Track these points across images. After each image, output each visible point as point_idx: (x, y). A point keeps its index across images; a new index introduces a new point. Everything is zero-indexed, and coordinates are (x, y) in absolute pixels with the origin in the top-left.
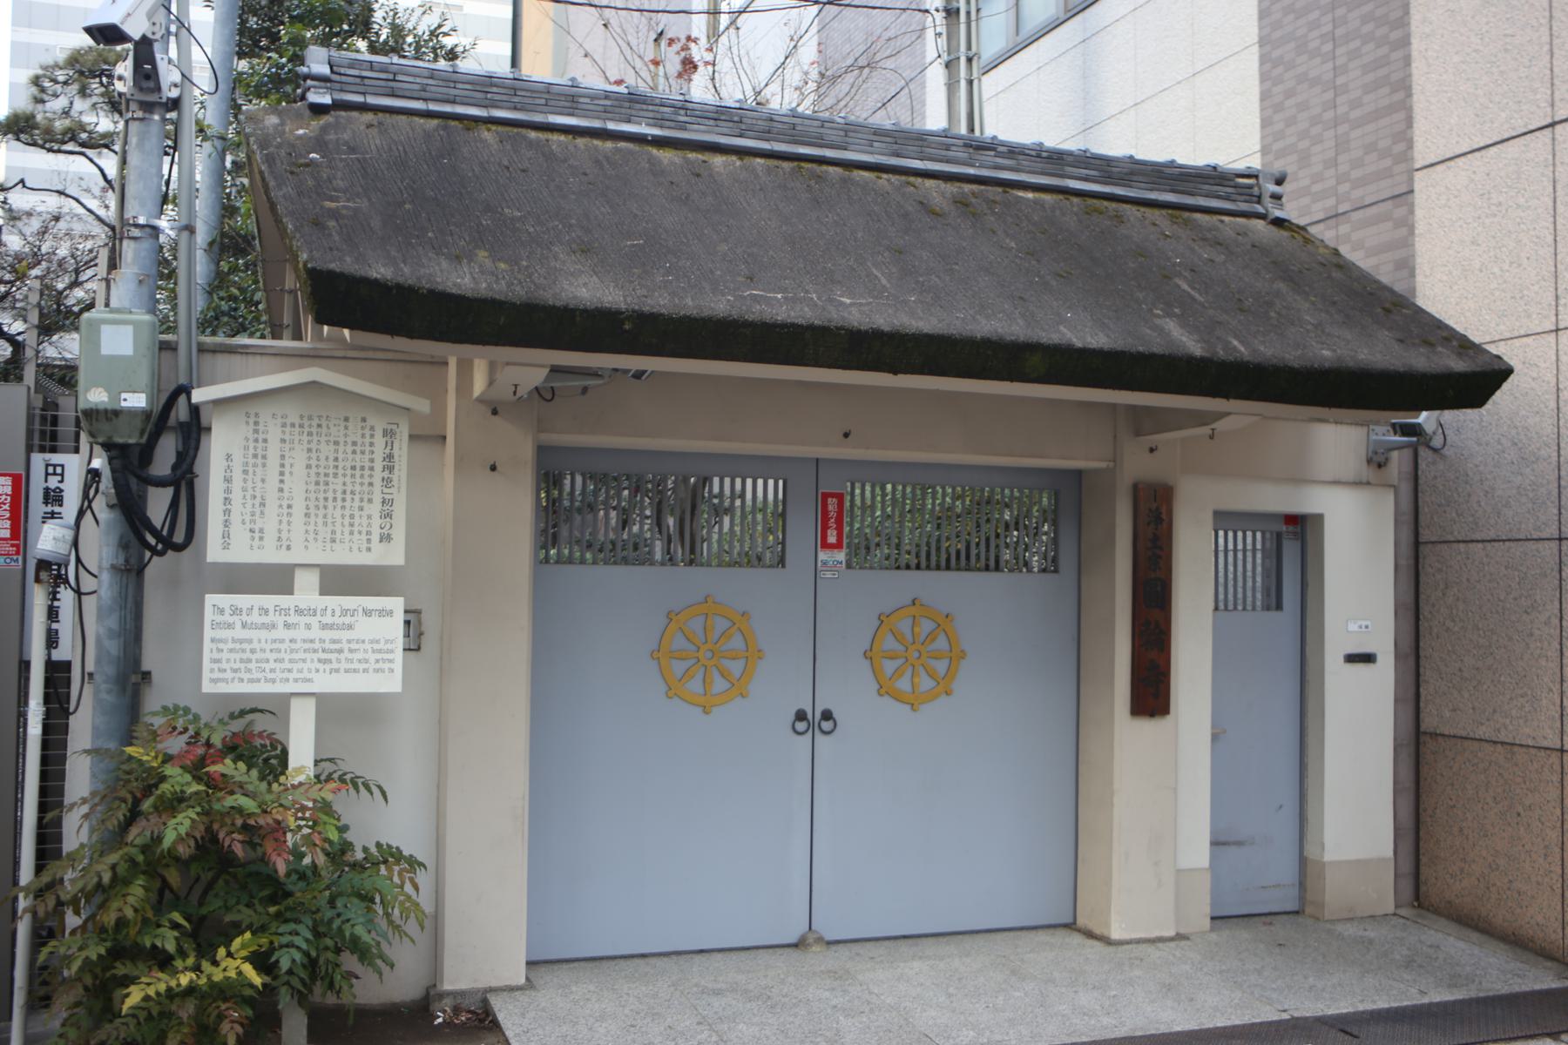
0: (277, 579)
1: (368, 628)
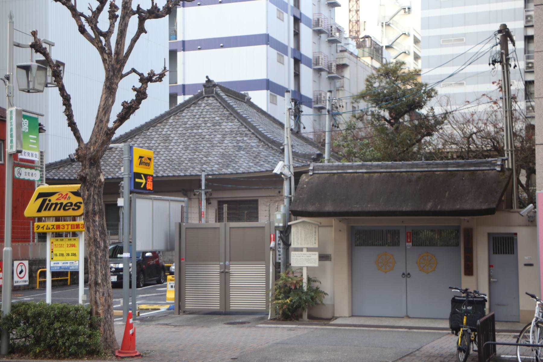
0: (301, 250)
1: (313, 257)
